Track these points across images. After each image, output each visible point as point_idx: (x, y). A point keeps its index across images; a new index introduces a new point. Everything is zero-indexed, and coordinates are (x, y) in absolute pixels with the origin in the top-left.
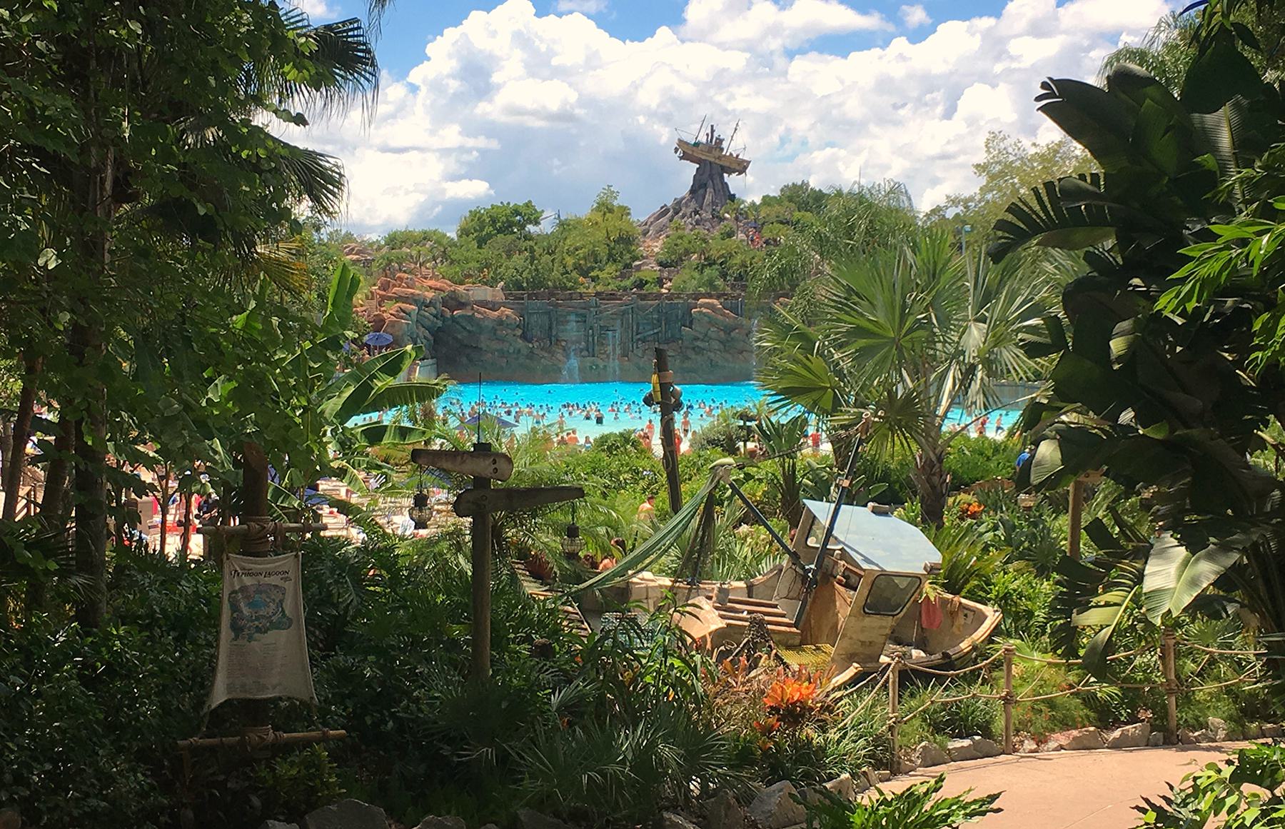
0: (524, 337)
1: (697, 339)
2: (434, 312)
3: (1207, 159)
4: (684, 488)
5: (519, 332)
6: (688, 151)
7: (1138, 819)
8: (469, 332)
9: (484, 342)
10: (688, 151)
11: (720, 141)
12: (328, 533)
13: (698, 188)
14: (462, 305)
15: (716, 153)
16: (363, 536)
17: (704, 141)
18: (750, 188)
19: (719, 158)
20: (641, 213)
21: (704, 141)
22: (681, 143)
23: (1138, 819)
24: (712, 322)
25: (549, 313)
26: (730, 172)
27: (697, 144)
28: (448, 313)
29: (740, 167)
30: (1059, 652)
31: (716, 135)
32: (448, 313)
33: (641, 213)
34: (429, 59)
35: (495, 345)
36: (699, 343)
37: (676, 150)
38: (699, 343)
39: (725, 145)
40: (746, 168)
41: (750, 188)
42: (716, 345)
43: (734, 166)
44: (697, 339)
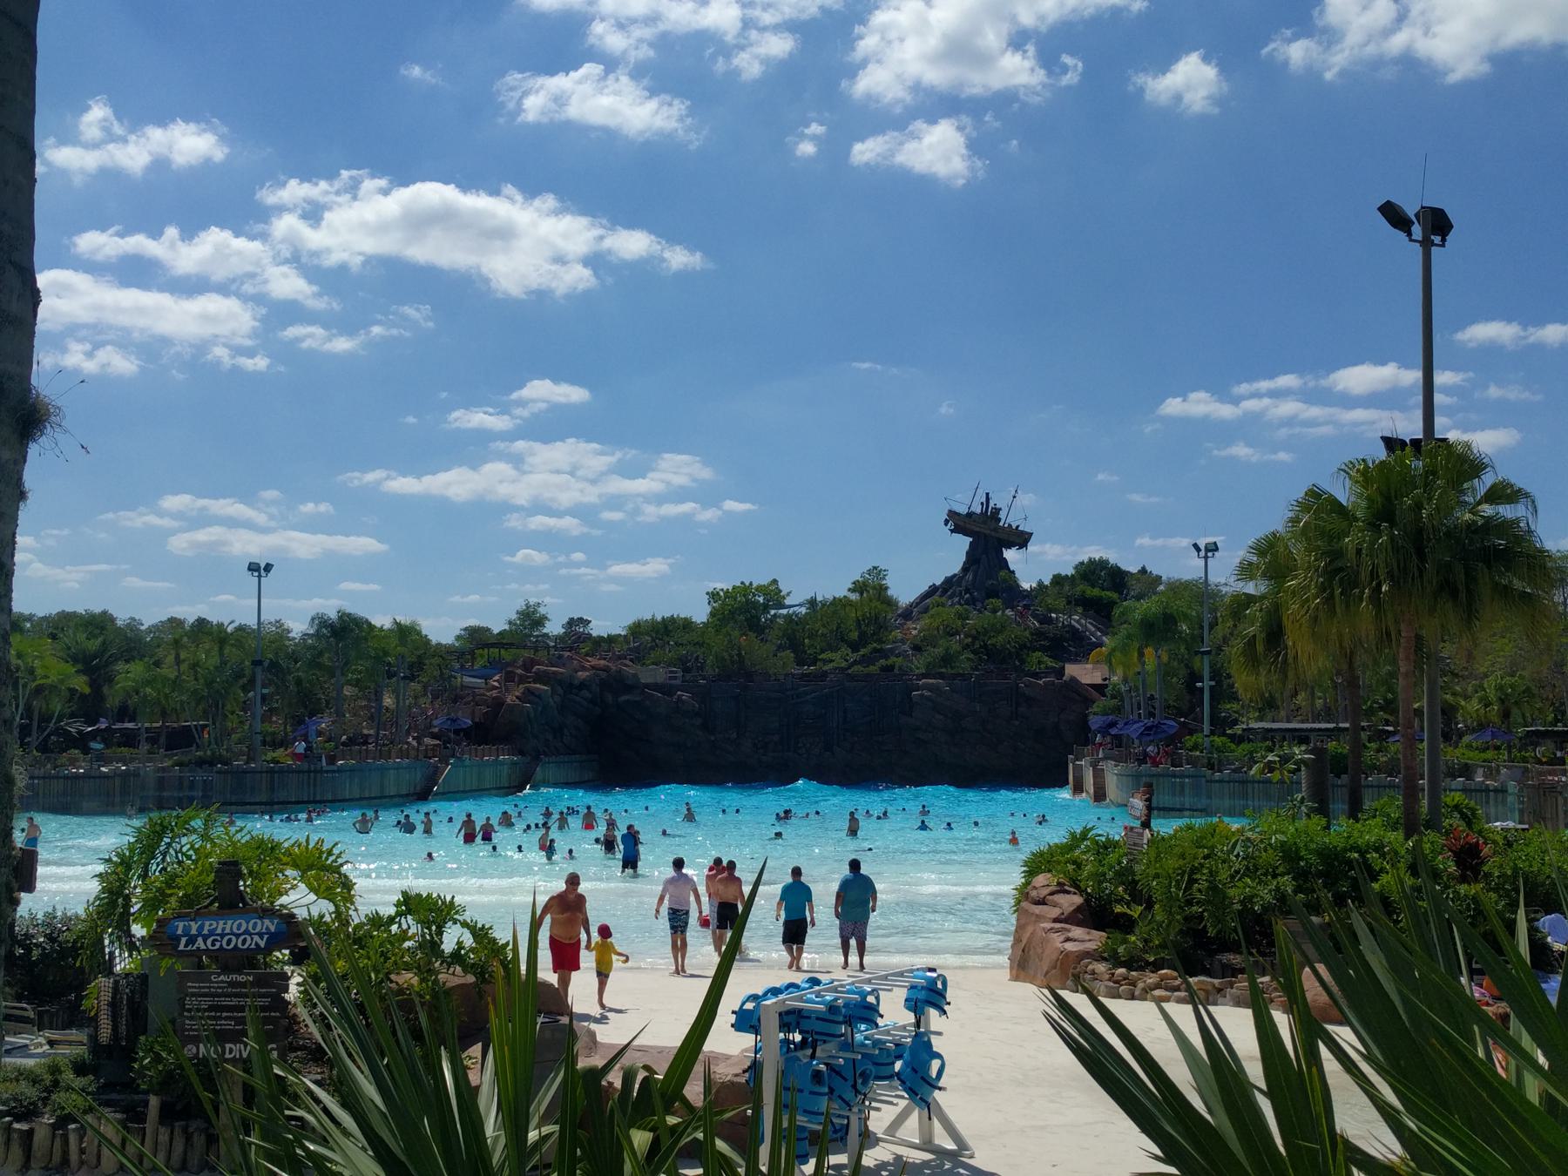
3: (172, 232)
4: (761, 888)
6: (959, 523)
10: (959, 523)
11: (997, 511)
12: (118, 1116)
14: (629, 688)
17: (978, 511)
18: (1030, 568)
21: (978, 511)
22: (952, 514)
27: (970, 515)
29: (1021, 539)
30: (1156, 1025)
31: (991, 505)
32: (609, 698)
34: (775, 581)
37: (946, 522)
39: (1002, 515)
41: (1030, 568)
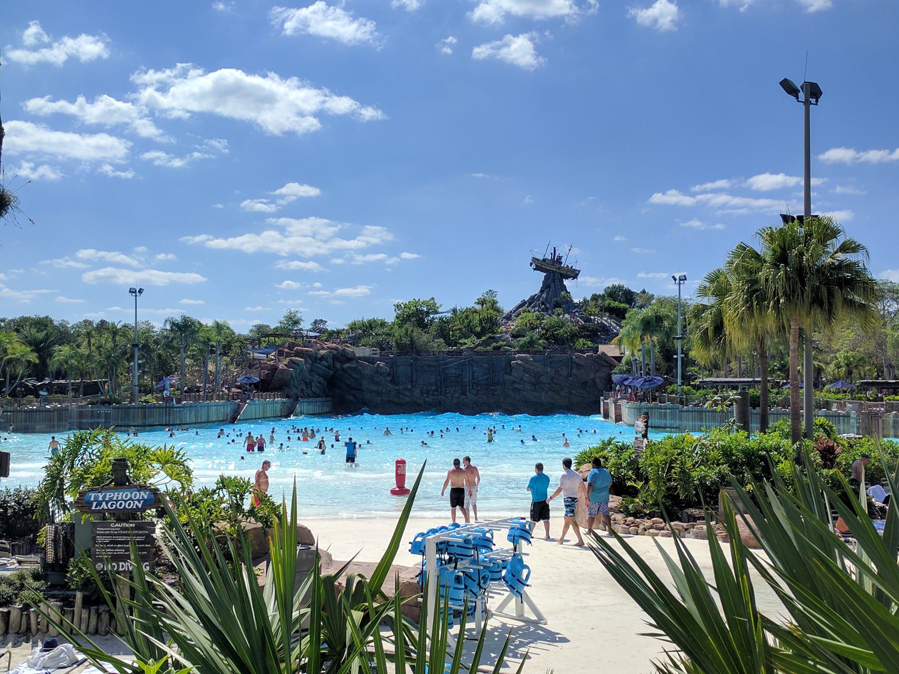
0: (393, 382)
1: (515, 382)
2: (326, 364)
5: (389, 378)
6: (539, 265)
7: (4, 489)
8: (355, 379)
9: (365, 384)
10: (539, 265)
11: (560, 258)
13: (546, 286)
14: (349, 360)
15: (558, 266)
16: (154, 510)
19: (559, 268)
20: (507, 305)
21: (550, 258)
22: (535, 260)
23: (4, 489)
24: (526, 371)
25: (411, 365)
26: (567, 277)
27: (544, 260)
28: (338, 365)
29: (574, 274)
31: (557, 254)
32: (338, 365)
33: (507, 305)
35: (373, 387)
36: (516, 386)
37: (531, 264)
38: (516, 386)
39: (563, 260)
40: (577, 275)
42: (528, 387)
43: (569, 273)
44: (515, 382)
